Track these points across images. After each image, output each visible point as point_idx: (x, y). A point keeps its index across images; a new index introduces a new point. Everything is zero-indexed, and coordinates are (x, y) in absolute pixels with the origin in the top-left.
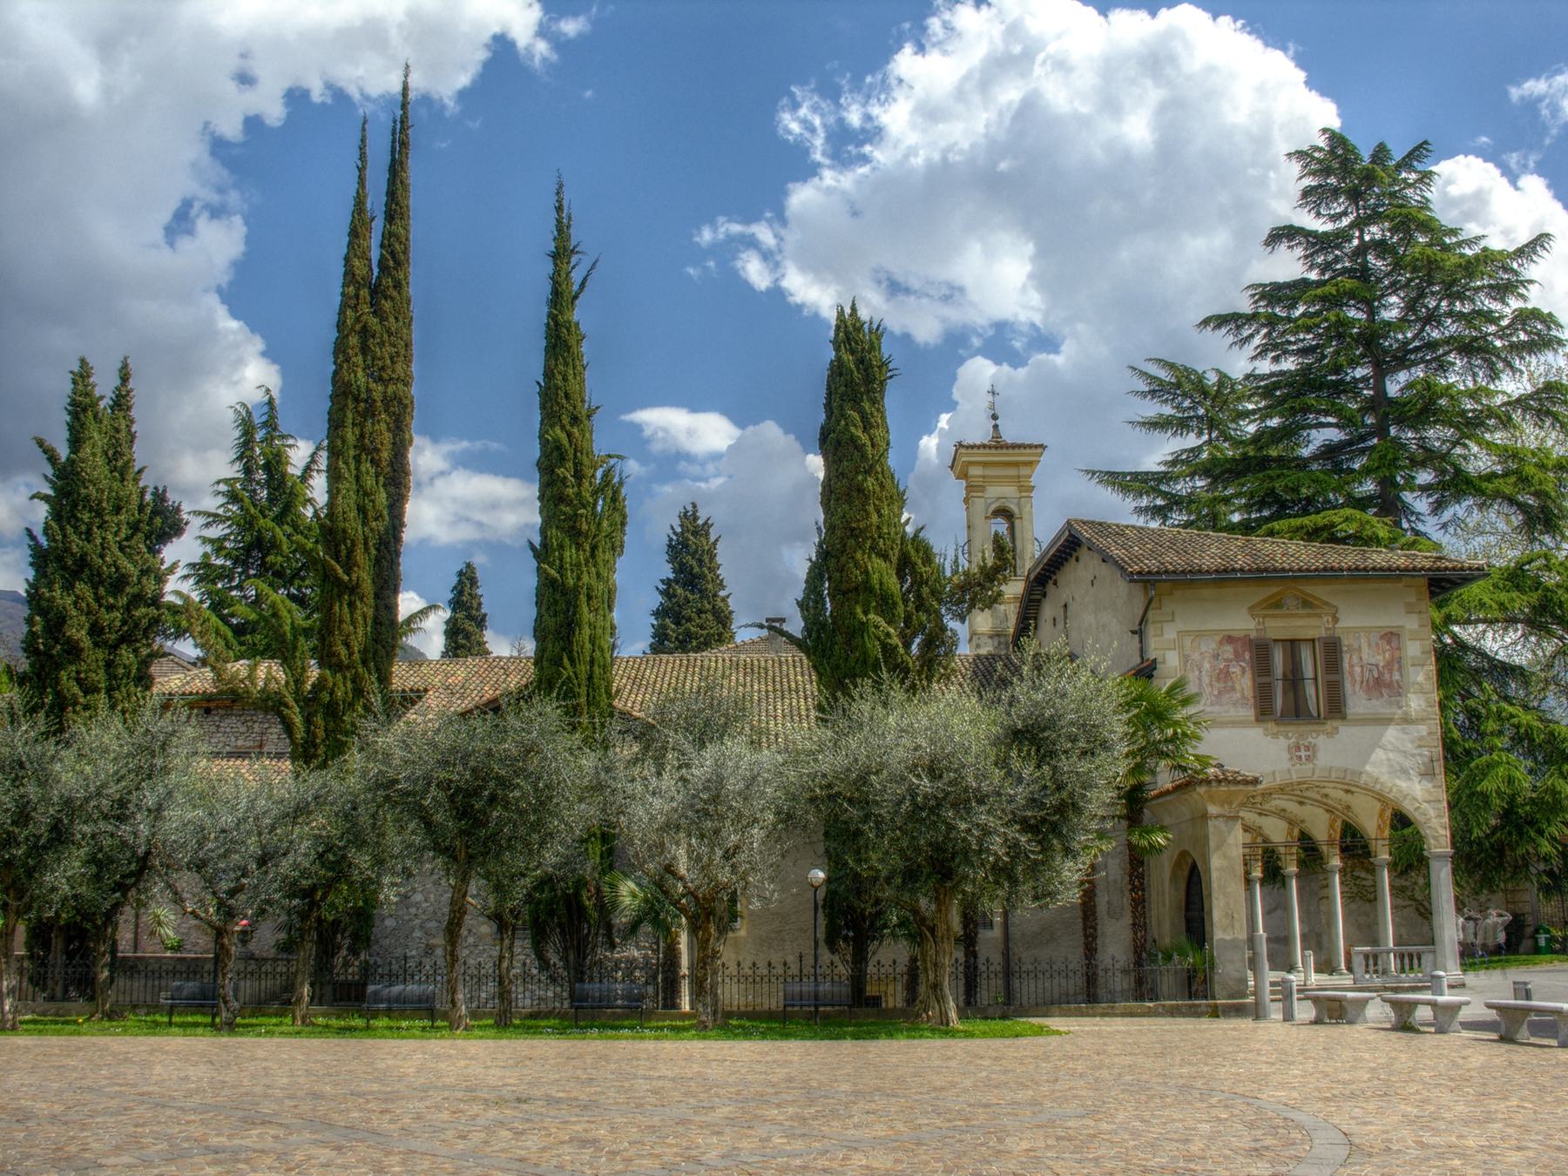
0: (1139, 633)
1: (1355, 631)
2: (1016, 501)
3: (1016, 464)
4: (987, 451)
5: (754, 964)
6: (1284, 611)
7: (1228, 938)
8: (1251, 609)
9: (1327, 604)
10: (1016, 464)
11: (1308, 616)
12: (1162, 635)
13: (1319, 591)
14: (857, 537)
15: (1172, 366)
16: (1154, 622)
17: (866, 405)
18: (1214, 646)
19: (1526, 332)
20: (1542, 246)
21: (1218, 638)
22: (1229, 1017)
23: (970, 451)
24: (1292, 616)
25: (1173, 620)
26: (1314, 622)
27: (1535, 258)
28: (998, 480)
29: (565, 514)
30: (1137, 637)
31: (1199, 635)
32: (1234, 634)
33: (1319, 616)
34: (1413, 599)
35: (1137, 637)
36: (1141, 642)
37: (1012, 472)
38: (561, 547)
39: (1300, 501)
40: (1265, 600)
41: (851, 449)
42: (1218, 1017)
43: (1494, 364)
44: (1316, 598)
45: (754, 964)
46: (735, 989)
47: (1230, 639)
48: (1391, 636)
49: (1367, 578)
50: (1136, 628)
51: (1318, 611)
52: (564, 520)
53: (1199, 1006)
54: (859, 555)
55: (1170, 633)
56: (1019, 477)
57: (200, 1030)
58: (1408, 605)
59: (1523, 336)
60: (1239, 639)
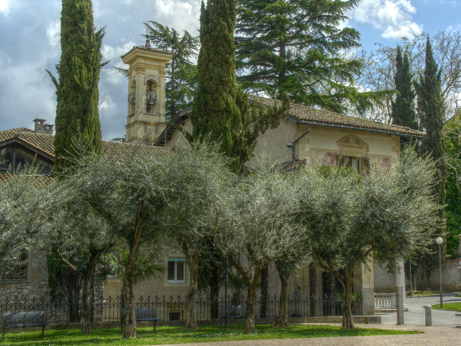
0: (292, 147)
1: (374, 156)
2: (158, 78)
3: (159, 61)
4: (143, 51)
5: (171, 297)
6: (350, 144)
7: (367, 287)
8: (338, 141)
9: (365, 143)
10: (159, 61)
11: (358, 147)
12: (304, 149)
13: (362, 137)
14: (223, 85)
15: (161, 27)
16: (301, 143)
17: (230, 20)
18: (323, 156)
19: (343, 38)
20: (355, 3)
21: (325, 153)
22: (372, 323)
23: (141, 51)
24: (352, 146)
25: (308, 143)
26: (359, 150)
27: (351, 8)
28: (150, 67)
29: (82, 50)
30: (291, 149)
31: (318, 151)
32: (332, 152)
33: (362, 148)
34: (395, 145)
35: (292, 149)
36: (293, 151)
37: (157, 64)
38: (80, 67)
39: (430, 94)
40: (343, 138)
41: (223, 41)
42: (367, 323)
43: (323, 49)
44: (361, 140)
45: (171, 297)
46: (116, 309)
47: (329, 154)
48: (387, 160)
49: (381, 133)
50: (290, 144)
51: (362, 146)
52: (82, 53)
53: (360, 318)
54: (224, 94)
55: (307, 149)
56: (160, 67)
57: (189, 339)
58: (393, 147)
59: (341, 40)
60: (333, 154)
